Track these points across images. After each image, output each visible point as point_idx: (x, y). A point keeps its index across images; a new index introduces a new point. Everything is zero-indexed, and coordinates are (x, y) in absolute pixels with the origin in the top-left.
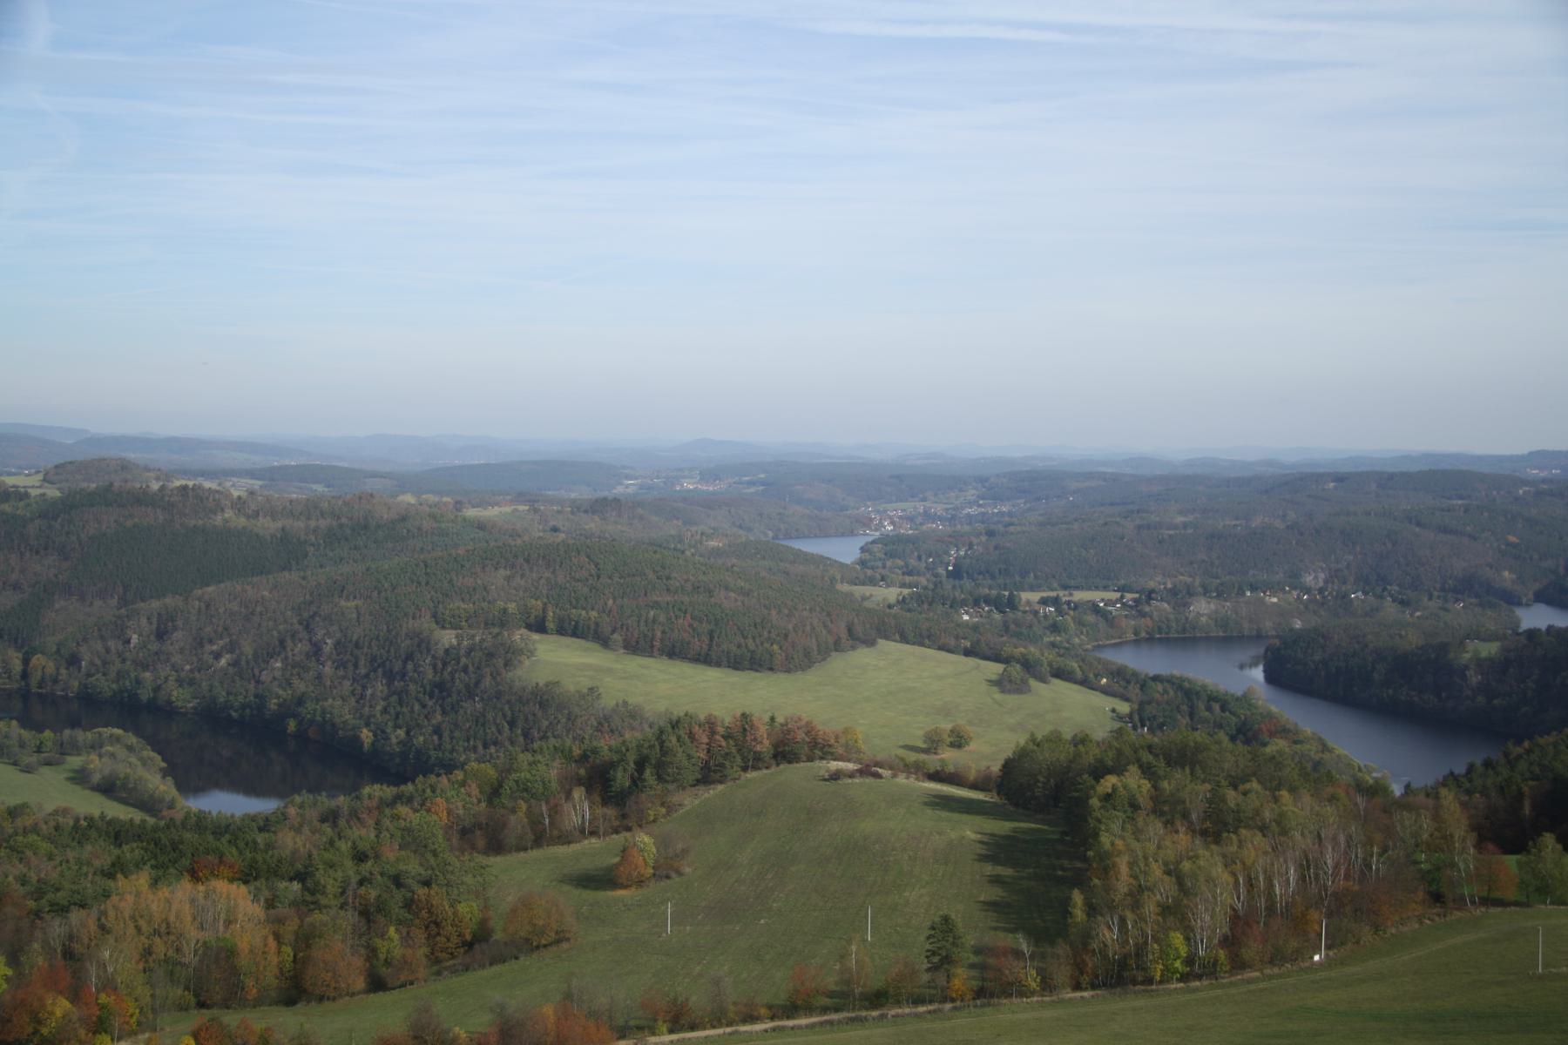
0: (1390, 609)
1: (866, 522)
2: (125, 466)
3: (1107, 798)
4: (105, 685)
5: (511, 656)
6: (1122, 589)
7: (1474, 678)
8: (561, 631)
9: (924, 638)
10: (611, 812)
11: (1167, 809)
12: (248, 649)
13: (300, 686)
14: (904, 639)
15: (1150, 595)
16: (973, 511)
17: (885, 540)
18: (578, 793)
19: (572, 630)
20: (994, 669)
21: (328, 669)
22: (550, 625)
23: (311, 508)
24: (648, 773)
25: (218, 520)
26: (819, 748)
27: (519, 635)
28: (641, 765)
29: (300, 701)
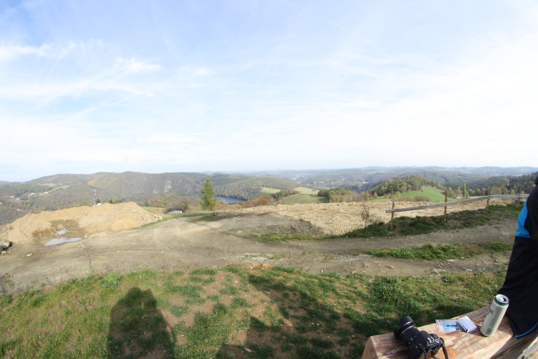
0: (351, 182)
1: (296, 176)
2: (219, 173)
3: (331, 193)
4: (220, 194)
5: (260, 189)
6: (324, 181)
7: (360, 188)
8: (265, 187)
9: (304, 186)
10: (275, 200)
11: (338, 194)
12: (233, 190)
13: (239, 193)
14: (302, 187)
15: (327, 182)
16: (253, 219)
17: (298, 178)
18: (272, 198)
19: (267, 187)
20: (312, 189)
21: (241, 191)
22: (264, 186)
23: (238, 176)
24: (280, 196)
25: (229, 177)
26: (298, 193)
27: (261, 187)
28: (278, 195)
29: (239, 195)
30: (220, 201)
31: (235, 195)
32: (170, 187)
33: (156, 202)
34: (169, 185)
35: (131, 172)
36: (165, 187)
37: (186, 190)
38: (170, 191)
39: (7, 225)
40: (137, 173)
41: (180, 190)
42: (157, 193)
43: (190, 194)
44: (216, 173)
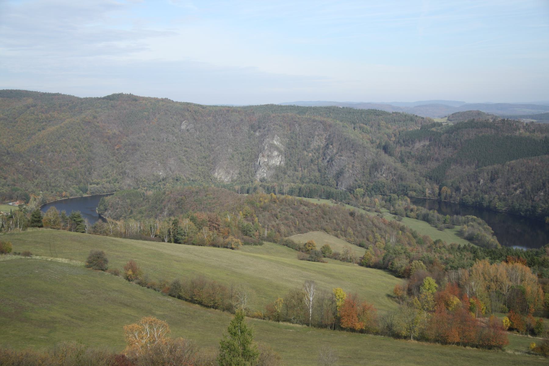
2: (479, 113)
4: (470, 199)
30: (466, 228)
31: (534, 208)
32: (277, 161)
33: (213, 225)
34: (276, 153)
35: (132, 99)
36: (262, 160)
37: (339, 174)
38: (279, 172)
39: (186, 159)
40: (157, 100)
41: (317, 174)
42: (226, 180)
43: (351, 190)
44: (463, 114)
